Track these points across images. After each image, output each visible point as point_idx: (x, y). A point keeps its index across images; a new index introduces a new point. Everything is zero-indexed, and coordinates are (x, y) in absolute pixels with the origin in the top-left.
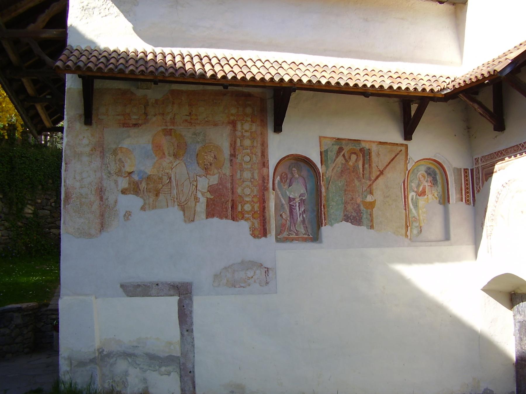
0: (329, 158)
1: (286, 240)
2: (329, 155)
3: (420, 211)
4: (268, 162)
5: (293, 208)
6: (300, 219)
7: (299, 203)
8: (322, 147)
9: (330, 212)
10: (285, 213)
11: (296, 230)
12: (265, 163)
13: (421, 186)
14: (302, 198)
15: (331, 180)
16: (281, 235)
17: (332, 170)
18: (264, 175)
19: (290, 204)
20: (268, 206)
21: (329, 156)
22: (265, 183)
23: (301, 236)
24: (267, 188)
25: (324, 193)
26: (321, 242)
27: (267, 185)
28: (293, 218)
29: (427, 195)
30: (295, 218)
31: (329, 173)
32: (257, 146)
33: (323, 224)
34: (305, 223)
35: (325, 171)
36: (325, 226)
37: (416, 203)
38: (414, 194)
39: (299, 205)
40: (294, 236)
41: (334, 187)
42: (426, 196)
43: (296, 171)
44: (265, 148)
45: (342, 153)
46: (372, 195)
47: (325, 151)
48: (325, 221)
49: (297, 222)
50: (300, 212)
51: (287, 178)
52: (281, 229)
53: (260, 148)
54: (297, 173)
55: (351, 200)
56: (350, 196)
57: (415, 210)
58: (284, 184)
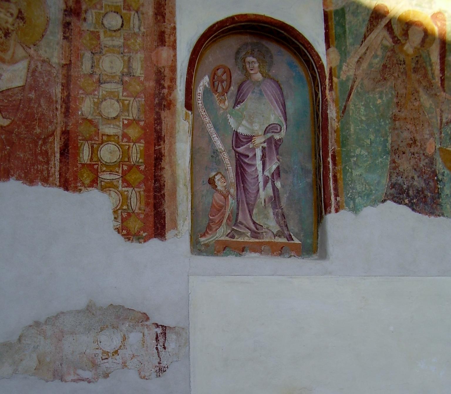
0: (347, 30)
4: (175, 33)
5: (245, 163)
7: (263, 148)
9: (352, 173)
10: (223, 177)
11: (254, 223)
14: (273, 136)
15: (355, 87)
16: (208, 236)
17: (358, 61)
18: (159, 66)
19: (236, 152)
20: (172, 151)
22: (164, 87)
23: (267, 240)
24: (171, 101)
28: (245, 189)
30: (252, 189)
33: (330, 205)
34: (279, 202)
36: (337, 211)
39: (263, 157)
40: (246, 239)
41: (362, 109)
43: (257, 65)
47: (336, 12)
48: (338, 199)
50: (267, 173)
51: (231, 82)
54: (257, 70)
55: (410, 146)
56: (406, 134)
58: (223, 97)
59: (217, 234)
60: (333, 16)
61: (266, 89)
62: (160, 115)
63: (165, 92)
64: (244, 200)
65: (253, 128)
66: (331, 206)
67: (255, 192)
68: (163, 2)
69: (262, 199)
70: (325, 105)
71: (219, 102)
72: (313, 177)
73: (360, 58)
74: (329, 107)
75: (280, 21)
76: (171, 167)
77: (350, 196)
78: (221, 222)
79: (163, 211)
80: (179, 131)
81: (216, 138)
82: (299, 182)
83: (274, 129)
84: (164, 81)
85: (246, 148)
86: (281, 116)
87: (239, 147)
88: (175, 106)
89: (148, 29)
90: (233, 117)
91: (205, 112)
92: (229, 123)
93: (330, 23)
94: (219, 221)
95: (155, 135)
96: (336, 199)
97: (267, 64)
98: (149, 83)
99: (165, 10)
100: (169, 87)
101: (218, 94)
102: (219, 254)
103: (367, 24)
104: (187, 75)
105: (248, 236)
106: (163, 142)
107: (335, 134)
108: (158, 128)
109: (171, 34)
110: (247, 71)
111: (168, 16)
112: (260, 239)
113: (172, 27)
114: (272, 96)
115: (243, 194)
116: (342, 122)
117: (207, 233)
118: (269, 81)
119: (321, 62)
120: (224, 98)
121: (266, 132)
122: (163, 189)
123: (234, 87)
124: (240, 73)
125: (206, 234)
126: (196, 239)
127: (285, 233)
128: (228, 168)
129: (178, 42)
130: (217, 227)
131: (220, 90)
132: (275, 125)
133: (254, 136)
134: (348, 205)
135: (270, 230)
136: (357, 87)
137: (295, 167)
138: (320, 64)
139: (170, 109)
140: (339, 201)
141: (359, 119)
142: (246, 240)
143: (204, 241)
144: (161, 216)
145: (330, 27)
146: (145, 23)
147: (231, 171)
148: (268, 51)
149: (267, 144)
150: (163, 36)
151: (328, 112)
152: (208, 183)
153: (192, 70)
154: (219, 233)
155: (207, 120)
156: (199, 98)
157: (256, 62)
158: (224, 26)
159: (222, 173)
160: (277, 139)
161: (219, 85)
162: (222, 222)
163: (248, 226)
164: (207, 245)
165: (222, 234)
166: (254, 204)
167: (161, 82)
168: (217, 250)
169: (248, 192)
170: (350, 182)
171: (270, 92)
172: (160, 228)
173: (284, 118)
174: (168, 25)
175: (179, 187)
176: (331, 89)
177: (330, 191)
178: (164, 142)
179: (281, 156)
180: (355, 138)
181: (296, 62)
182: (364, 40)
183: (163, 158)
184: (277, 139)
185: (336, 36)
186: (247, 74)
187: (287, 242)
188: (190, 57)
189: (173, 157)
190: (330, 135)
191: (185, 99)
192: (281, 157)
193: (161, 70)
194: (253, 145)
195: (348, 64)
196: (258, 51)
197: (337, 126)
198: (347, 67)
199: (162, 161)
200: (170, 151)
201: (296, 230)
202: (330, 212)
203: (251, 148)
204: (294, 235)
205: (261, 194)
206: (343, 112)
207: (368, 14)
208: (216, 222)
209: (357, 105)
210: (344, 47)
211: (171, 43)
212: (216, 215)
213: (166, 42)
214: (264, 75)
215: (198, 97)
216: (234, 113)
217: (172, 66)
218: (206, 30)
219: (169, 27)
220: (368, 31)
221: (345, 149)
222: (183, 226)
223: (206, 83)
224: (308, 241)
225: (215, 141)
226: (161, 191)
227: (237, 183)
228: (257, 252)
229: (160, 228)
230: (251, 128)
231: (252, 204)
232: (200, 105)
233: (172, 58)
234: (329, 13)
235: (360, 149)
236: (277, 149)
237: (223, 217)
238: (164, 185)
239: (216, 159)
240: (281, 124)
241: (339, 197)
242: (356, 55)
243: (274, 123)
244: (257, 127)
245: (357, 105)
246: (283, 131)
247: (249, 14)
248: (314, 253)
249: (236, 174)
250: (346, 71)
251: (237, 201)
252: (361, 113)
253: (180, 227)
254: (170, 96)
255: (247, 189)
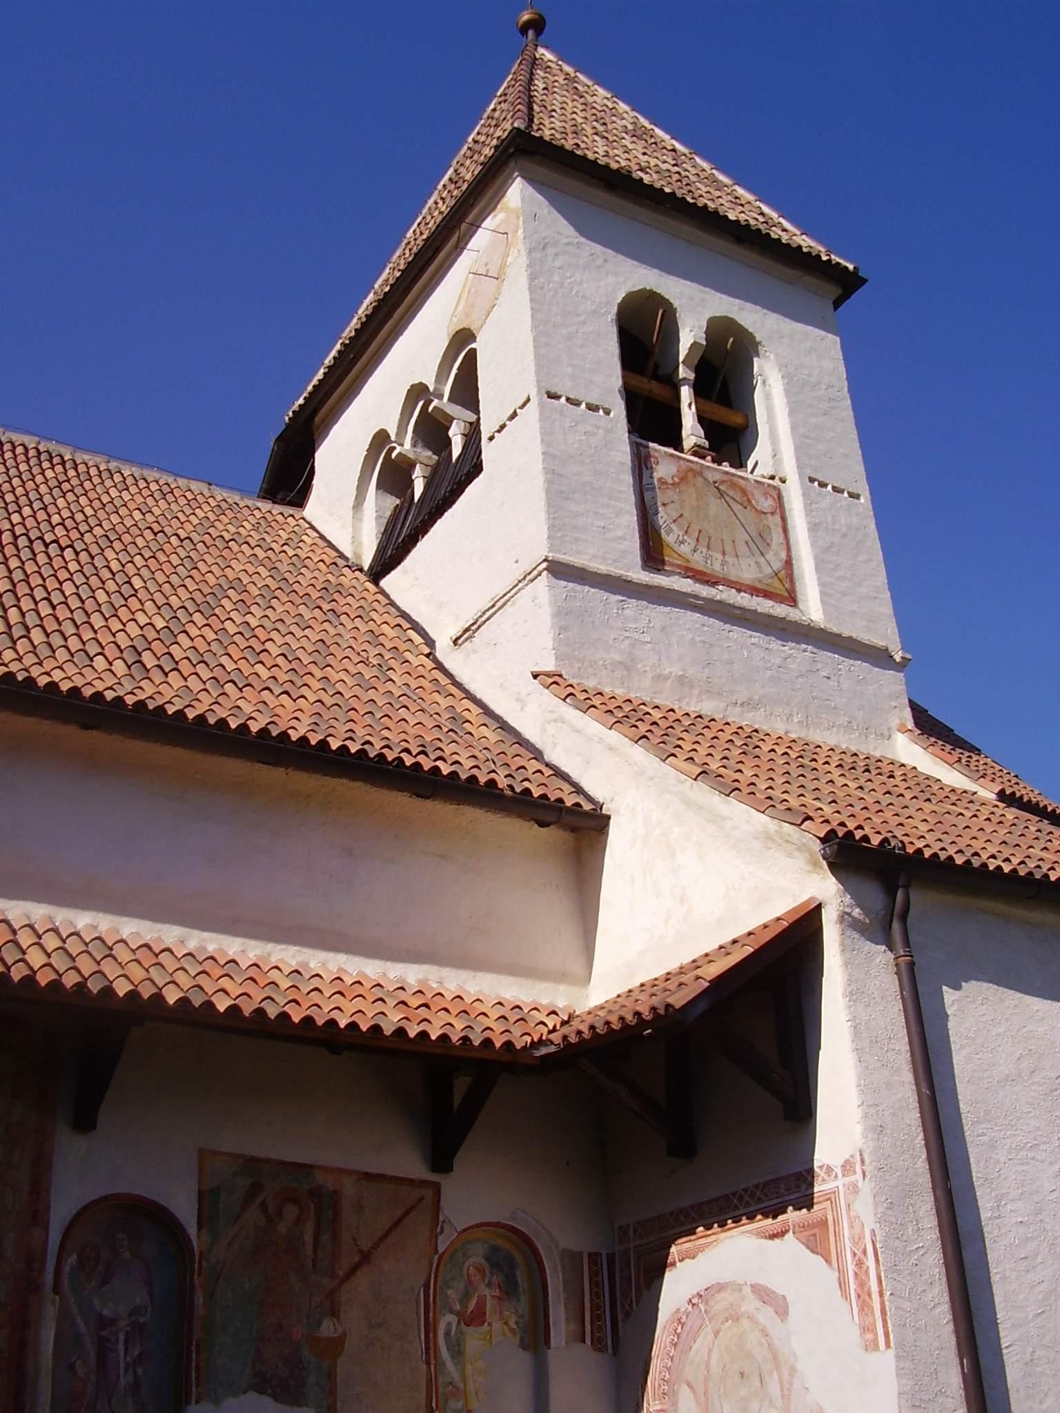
3: (469, 1367)
6: (124, 1380)
7: (127, 1334)
13: (472, 1296)
29: (490, 1324)
37: (459, 1345)
38: (452, 1318)
39: (126, 1341)
42: (486, 1324)
45: (259, 1200)
46: (335, 1320)
57: (455, 1364)
81: (79, 1320)
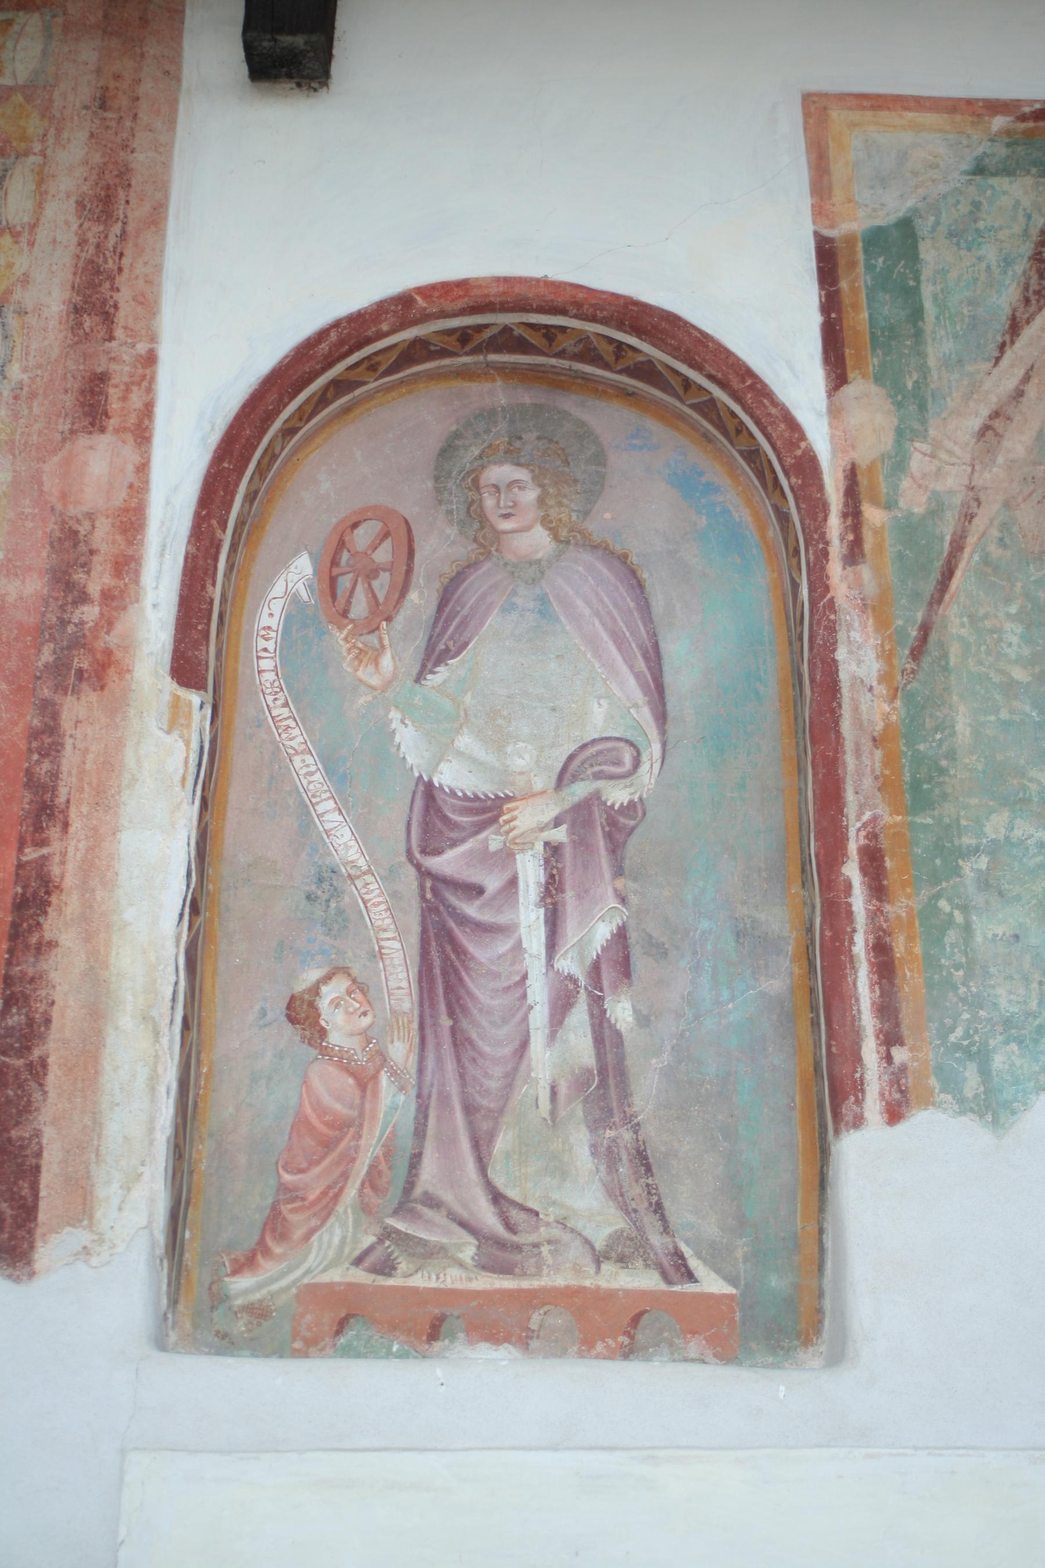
0: (928, 305)
1: (341, 1326)
2: (926, 273)
4: (152, 380)
5: (463, 921)
7: (553, 850)
8: (838, 196)
9: (967, 929)
10: (359, 987)
11: (497, 1198)
12: (114, 393)
14: (597, 795)
15: (971, 540)
16: (268, 1268)
17: (985, 429)
18: (72, 511)
19: (424, 873)
21: (927, 291)
22: (83, 598)
23: (560, 1281)
24: (108, 652)
25: (865, 701)
26: (836, 1358)
27: (108, 623)
28: (460, 1041)
31: (939, 474)
32: (33, 227)
33: (859, 1087)
34: (625, 1095)
35: (888, 441)
36: (894, 1115)
40: (453, 1279)
41: (1013, 632)
43: (530, 496)
44: (123, 236)
47: (876, 238)
48: (900, 1055)
49: (522, 1090)
50: (568, 964)
51: (409, 571)
52: (287, 1177)
53: (68, 238)
54: (532, 514)
58: (373, 639)
59: (311, 1257)
60: (861, 256)
61: (571, 592)
62: (55, 716)
63: (85, 618)
64: (453, 1088)
65: (509, 762)
66: (863, 1091)
67: (507, 1050)
68: (110, 261)
69: (542, 1083)
70: (826, 628)
71: (356, 658)
72: (797, 971)
73: (996, 415)
74: (841, 635)
75: (616, 296)
76: (88, 937)
77: (964, 1038)
78: (331, 1197)
79: (30, 1139)
80: (134, 780)
82: (725, 995)
83: (605, 763)
84: (88, 573)
85: (471, 852)
86: (640, 702)
87: (438, 852)
88: (125, 671)
89: (39, 372)
90: (413, 722)
91: (286, 705)
92: (394, 750)
93: (844, 285)
94: (324, 1193)
95: (26, 800)
96: (889, 1058)
97: (579, 488)
98: (23, 582)
99: (118, 290)
100: (107, 596)
101: (350, 627)
102: (312, 1349)
103: (1024, 273)
104: (189, 542)
105: (461, 1264)
106: (58, 829)
107: (878, 754)
108: (46, 766)
109: (133, 383)
110: (483, 520)
111: (124, 316)
112: (524, 1275)
113: (141, 356)
114: (597, 622)
115: (450, 1066)
116: (909, 698)
117: (267, 1252)
118: (587, 557)
119: (803, 445)
120: (376, 641)
121: (568, 776)
122: (42, 1038)
123: (421, 593)
124: (452, 531)
125: (259, 1257)
126: (212, 1283)
127: (652, 1247)
128: (381, 948)
129: (160, 412)
130: (314, 1222)
131: (360, 608)
132: (609, 745)
133: (508, 799)
134: (952, 1084)
135: (572, 1231)
136: (979, 539)
137: (705, 924)
138: (799, 453)
139: (102, 688)
140: (903, 1069)
141: (996, 679)
142: (449, 1284)
143: (246, 1292)
144: (22, 1164)
145: (846, 300)
146: (27, 347)
147: (396, 962)
148: (584, 434)
149: (571, 832)
150: (101, 393)
151: (841, 654)
152: (283, 1018)
153: (214, 522)
154: (320, 1248)
155: (296, 738)
156: (265, 650)
157: (530, 484)
158: (369, 333)
159: (355, 972)
160: (616, 807)
161: (359, 588)
162: (337, 1197)
163: (464, 1214)
164: (259, 1312)
165: (331, 1254)
166: (501, 1111)
167: (76, 577)
168: (308, 1334)
169: (471, 1053)
170: (961, 973)
171: (588, 603)
172: (9, 1221)
173: (652, 709)
174: (124, 348)
175: (117, 1028)
176: (854, 553)
177: (855, 1019)
178: (66, 825)
179: (635, 879)
180: (980, 767)
181: (714, 473)
182: (1007, 338)
183: (54, 899)
184: (616, 807)
185: (872, 334)
186: (484, 537)
187: (663, 1286)
188: (208, 471)
189: (99, 895)
190: (850, 760)
191: (175, 641)
192: (631, 884)
193: (76, 527)
194: (502, 838)
195: (937, 445)
196: (539, 438)
197: (886, 716)
198: (933, 456)
199: (46, 913)
200: (88, 868)
201: (711, 1229)
202: (858, 1122)
203: (495, 853)
204: (698, 1255)
205: (534, 1063)
206: (917, 653)
207: (1026, 233)
208: (312, 1197)
209: (986, 616)
210: (915, 377)
211: (133, 419)
212: (312, 1164)
213: (108, 417)
214: (564, 533)
215: (262, 644)
216: (416, 700)
217: (126, 510)
218: (286, 357)
219: (125, 357)
220: (1027, 301)
221: (929, 821)
222: (120, 1209)
223: (300, 586)
224: (774, 1281)
225: (326, 832)
226: (29, 1049)
227: (421, 1017)
228: (507, 1339)
229: (9, 1221)
230: (497, 764)
231: (490, 1111)
232: (270, 676)
233: (130, 476)
234: (838, 244)
235: (1006, 814)
236: (615, 848)
237: (345, 1176)
238: (48, 1021)
239: (328, 907)
240: (640, 741)
241: (902, 1044)
242: (972, 404)
243: (605, 735)
244: (527, 756)
245: (986, 616)
246: (645, 767)
247: (477, 279)
248: (807, 1342)
249: (420, 972)
250: (924, 476)
251: (419, 1096)
252: (1008, 651)
253: (106, 1215)
254: (108, 633)
255: (470, 1042)
